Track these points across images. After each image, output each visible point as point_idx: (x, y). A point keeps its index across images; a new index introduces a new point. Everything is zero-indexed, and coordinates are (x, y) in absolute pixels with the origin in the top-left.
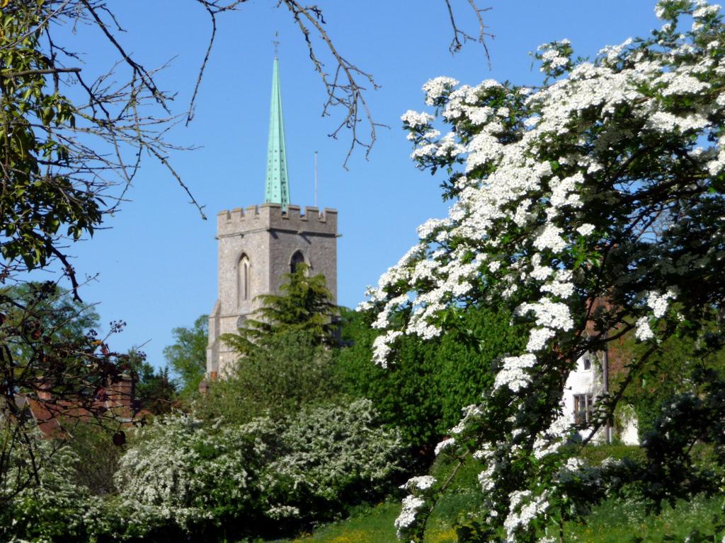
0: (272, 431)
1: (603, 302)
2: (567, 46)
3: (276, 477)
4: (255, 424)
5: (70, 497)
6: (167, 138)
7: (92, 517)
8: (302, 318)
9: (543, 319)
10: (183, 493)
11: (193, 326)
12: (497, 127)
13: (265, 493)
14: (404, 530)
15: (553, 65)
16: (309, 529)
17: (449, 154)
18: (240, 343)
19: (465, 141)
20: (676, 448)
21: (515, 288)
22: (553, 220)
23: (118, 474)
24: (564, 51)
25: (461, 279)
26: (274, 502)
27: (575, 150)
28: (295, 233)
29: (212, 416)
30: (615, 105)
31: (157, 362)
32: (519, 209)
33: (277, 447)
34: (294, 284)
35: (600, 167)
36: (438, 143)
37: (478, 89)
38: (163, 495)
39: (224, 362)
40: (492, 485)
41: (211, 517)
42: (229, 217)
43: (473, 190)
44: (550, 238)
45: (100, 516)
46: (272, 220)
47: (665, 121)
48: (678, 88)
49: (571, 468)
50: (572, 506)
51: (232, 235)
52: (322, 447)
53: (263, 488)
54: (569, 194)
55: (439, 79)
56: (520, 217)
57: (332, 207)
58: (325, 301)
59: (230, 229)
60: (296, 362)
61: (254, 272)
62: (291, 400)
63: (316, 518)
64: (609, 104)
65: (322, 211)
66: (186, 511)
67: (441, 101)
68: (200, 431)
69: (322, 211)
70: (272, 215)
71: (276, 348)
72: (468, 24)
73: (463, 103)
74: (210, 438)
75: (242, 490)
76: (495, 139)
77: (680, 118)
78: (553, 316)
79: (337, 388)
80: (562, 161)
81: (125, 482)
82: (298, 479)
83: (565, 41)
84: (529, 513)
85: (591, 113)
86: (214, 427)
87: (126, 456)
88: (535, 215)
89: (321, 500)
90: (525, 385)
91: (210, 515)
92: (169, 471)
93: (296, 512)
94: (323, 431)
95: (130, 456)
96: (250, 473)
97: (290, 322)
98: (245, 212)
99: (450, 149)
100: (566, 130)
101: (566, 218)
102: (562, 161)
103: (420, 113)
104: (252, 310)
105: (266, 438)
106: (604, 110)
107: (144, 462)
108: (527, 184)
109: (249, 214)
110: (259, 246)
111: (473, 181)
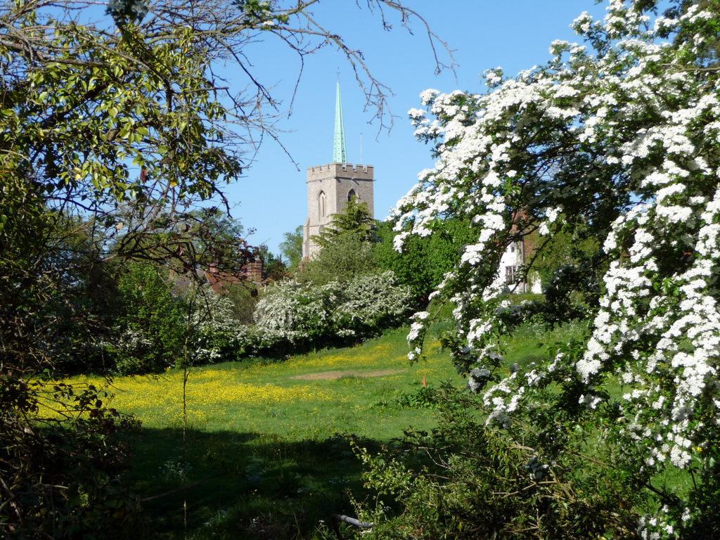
0: (339, 289)
2: (500, 71)
3: (342, 314)
7: (242, 336)
8: (355, 226)
9: (488, 223)
13: (336, 323)
15: (492, 82)
19: (444, 125)
20: (562, 294)
21: (472, 207)
22: (493, 169)
23: (255, 313)
24: (499, 73)
26: (340, 328)
27: (505, 129)
29: (306, 281)
30: (527, 103)
33: (342, 297)
34: (350, 207)
35: (519, 138)
39: (312, 251)
44: (492, 179)
46: (337, 172)
47: (555, 112)
49: (504, 306)
50: (505, 327)
52: (367, 297)
56: (475, 167)
57: (370, 165)
59: (314, 178)
60: (351, 251)
61: (327, 201)
63: (364, 336)
65: (365, 167)
66: (293, 333)
67: (430, 102)
68: (300, 289)
69: (365, 167)
70: (337, 169)
72: (444, 58)
73: (443, 104)
75: (323, 321)
76: (460, 123)
79: (374, 265)
80: (498, 135)
81: (259, 317)
82: (354, 315)
83: (499, 68)
84: (480, 331)
85: (514, 108)
87: (260, 303)
88: (483, 166)
90: (478, 261)
91: (306, 335)
92: (283, 311)
93: (353, 333)
95: (261, 304)
96: (328, 312)
99: (435, 130)
100: (500, 118)
102: (498, 135)
103: (418, 109)
105: (336, 293)
107: (269, 306)
110: (331, 187)
111: (449, 147)
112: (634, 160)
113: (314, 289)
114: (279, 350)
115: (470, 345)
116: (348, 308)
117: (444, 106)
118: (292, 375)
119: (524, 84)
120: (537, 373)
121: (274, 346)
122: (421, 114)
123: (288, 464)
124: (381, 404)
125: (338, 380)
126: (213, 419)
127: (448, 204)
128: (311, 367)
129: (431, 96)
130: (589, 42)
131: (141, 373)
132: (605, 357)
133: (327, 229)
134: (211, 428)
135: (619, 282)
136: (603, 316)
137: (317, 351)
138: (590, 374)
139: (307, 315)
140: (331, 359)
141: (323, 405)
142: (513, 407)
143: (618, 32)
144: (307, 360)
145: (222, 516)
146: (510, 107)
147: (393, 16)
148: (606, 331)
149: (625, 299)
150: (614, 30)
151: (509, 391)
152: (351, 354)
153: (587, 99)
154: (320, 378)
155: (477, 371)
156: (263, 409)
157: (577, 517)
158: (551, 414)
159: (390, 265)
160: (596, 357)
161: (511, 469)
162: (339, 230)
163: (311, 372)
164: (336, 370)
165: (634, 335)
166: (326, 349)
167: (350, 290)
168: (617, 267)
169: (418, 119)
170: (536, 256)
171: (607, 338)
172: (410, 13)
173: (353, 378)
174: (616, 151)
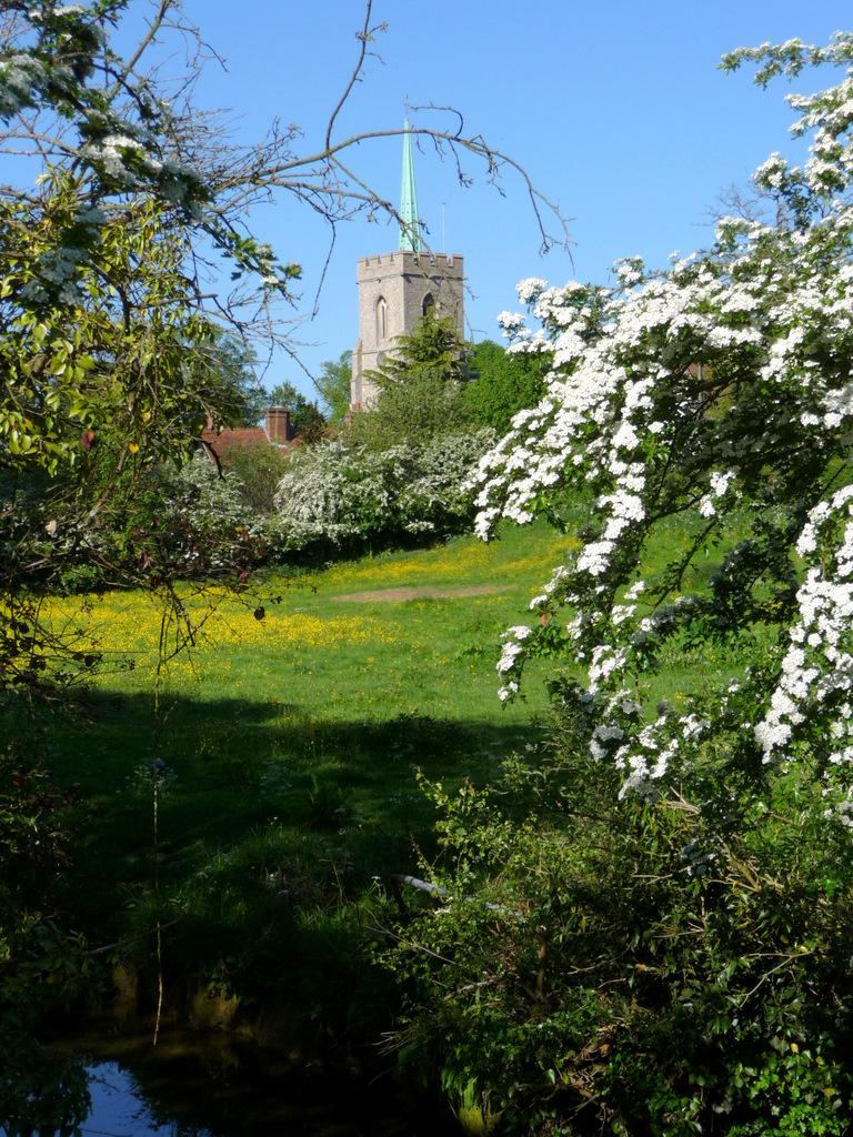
0: (409, 457)
1: (675, 474)
2: (639, 261)
3: (414, 496)
4: (394, 451)
5: (237, 516)
6: (292, 336)
7: (256, 533)
8: (433, 356)
9: (618, 509)
10: (333, 511)
11: (339, 361)
12: (581, 326)
13: (404, 511)
14: (504, 673)
15: (627, 280)
16: (443, 541)
17: (539, 349)
18: (379, 380)
19: (553, 337)
20: (739, 587)
21: (596, 472)
22: (628, 419)
23: (277, 495)
24: (637, 265)
25: (549, 470)
26: (411, 518)
27: (645, 358)
29: (356, 445)
30: (678, 328)
31: (311, 395)
32: (598, 410)
33: (413, 471)
34: (426, 325)
35: (668, 373)
36: (529, 340)
37: (564, 291)
38: (316, 514)
39: (366, 395)
40: (579, 634)
41: (358, 532)
42: (368, 264)
43: (560, 384)
44: (626, 436)
45: (263, 532)
46: (405, 266)
47: (722, 336)
48: (735, 306)
49: (644, 629)
50: (646, 662)
51: (370, 280)
52: (453, 470)
53: (402, 507)
54: (640, 396)
55: (530, 280)
56: (599, 417)
57: (459, 254)
58: (454, 340)
59: (368, 275)
60: (428, 396)
61: (390, 313)
62: (425, 430)
63: (449, 531)
64: (673, 327)
65: (450, 257)
66: (336, 527)
67: (532, 300)
68: (347, 458)
69: (450, 257)
70: (405, 261)
71: (411, 383)
72: (554, 229)
73: (551, 304)
74: (355, 463)
75: (384, 508)
76: (579, 338)
77: (736, 331)
78: (627, 507)
79: (465, 418)
80: (635, 368)
81: (283, 502)
82: (433, 498)
83: (637, 258)
84: (609, 665)
85: (660, 330)
86: (359, 454)
87: (284, 481)
88: (613, 413)
89: (452, 516)
90: (603, 569)
91: (357, 530)
92: (320, 493)
93: (432, 526)
94: (453, 456)
95: (286, 481)
96: (391, 494)
97: (422, 360)
98: (382, 260)
99: (540, 346)
100: (638, 343)
101: (639, 418)
102: (635, 368)
103: (513, 313)
104: (389, 347)
105: (404, 463)
106: (669, 331)
107: (298, 485)
108: (605, 389)
109: (385, 261)
110: (395, 290)
111: (561, 376)
112: (842, 421)
113: (369, 457)
114: (315, 554)
115: (593, 689)
116: (423, 487)
117: (553, 308)
118: (337, 594)
119: (676, 286)
120: (697, 719)
121: (307, 548)
122: (517, 321)
123: (332, 764)
124: (472, 652)
125: (408, 604)
126: (211, 676)
127: (557, 472)
128: (365, 581)
129: (532, 290)
130: (782, 199)
131: (101, 589)
132: (798, 718)
133: (390, 360)
134: (208, 693)
135: (819, 603)
136: (795, 656)
137: (374, 555)
138: (775, 745)
139: (358, 498)
140: (396, 567)
141: (382, 652)
142: (660, 770)
143: (826, 188)
144: (359, 570)
145: (223, 860)
146: (653, 328)
147: (475, 164)
148: (800, 679)
149: (829, 630)
150: (820, 185)
151: (654, 747)
152: (428, 560)
153: (772, 313)
154: (380, 599)
155: (604, 731)
156: (289, 658)
157: (763, 914)
158: (720, 779)
159: (490, 419)
160: (784, 719)
161: (662, 842)
162: (410, 362)
163: (366, 590)
164: (405, 585)
165: (844, 681)
166: (388, 552)
167: (427, 459)
168: (818, 579)
169: (513, 328)
170: (695, 549)
171: (800, 691)
172: (501, 160)
173: (431, 601)
174: (815, 405)
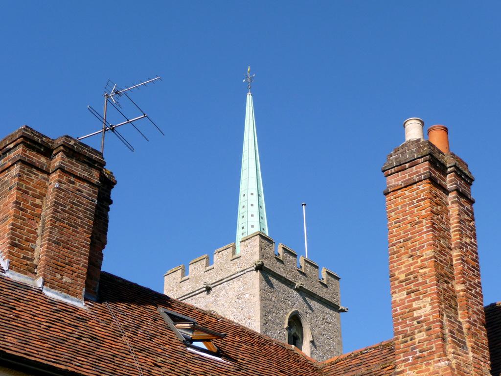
28: (290, 284)
46: (262, 256)
